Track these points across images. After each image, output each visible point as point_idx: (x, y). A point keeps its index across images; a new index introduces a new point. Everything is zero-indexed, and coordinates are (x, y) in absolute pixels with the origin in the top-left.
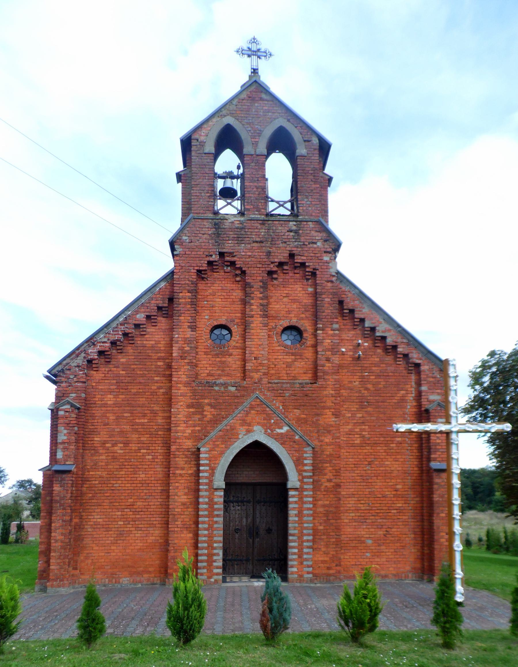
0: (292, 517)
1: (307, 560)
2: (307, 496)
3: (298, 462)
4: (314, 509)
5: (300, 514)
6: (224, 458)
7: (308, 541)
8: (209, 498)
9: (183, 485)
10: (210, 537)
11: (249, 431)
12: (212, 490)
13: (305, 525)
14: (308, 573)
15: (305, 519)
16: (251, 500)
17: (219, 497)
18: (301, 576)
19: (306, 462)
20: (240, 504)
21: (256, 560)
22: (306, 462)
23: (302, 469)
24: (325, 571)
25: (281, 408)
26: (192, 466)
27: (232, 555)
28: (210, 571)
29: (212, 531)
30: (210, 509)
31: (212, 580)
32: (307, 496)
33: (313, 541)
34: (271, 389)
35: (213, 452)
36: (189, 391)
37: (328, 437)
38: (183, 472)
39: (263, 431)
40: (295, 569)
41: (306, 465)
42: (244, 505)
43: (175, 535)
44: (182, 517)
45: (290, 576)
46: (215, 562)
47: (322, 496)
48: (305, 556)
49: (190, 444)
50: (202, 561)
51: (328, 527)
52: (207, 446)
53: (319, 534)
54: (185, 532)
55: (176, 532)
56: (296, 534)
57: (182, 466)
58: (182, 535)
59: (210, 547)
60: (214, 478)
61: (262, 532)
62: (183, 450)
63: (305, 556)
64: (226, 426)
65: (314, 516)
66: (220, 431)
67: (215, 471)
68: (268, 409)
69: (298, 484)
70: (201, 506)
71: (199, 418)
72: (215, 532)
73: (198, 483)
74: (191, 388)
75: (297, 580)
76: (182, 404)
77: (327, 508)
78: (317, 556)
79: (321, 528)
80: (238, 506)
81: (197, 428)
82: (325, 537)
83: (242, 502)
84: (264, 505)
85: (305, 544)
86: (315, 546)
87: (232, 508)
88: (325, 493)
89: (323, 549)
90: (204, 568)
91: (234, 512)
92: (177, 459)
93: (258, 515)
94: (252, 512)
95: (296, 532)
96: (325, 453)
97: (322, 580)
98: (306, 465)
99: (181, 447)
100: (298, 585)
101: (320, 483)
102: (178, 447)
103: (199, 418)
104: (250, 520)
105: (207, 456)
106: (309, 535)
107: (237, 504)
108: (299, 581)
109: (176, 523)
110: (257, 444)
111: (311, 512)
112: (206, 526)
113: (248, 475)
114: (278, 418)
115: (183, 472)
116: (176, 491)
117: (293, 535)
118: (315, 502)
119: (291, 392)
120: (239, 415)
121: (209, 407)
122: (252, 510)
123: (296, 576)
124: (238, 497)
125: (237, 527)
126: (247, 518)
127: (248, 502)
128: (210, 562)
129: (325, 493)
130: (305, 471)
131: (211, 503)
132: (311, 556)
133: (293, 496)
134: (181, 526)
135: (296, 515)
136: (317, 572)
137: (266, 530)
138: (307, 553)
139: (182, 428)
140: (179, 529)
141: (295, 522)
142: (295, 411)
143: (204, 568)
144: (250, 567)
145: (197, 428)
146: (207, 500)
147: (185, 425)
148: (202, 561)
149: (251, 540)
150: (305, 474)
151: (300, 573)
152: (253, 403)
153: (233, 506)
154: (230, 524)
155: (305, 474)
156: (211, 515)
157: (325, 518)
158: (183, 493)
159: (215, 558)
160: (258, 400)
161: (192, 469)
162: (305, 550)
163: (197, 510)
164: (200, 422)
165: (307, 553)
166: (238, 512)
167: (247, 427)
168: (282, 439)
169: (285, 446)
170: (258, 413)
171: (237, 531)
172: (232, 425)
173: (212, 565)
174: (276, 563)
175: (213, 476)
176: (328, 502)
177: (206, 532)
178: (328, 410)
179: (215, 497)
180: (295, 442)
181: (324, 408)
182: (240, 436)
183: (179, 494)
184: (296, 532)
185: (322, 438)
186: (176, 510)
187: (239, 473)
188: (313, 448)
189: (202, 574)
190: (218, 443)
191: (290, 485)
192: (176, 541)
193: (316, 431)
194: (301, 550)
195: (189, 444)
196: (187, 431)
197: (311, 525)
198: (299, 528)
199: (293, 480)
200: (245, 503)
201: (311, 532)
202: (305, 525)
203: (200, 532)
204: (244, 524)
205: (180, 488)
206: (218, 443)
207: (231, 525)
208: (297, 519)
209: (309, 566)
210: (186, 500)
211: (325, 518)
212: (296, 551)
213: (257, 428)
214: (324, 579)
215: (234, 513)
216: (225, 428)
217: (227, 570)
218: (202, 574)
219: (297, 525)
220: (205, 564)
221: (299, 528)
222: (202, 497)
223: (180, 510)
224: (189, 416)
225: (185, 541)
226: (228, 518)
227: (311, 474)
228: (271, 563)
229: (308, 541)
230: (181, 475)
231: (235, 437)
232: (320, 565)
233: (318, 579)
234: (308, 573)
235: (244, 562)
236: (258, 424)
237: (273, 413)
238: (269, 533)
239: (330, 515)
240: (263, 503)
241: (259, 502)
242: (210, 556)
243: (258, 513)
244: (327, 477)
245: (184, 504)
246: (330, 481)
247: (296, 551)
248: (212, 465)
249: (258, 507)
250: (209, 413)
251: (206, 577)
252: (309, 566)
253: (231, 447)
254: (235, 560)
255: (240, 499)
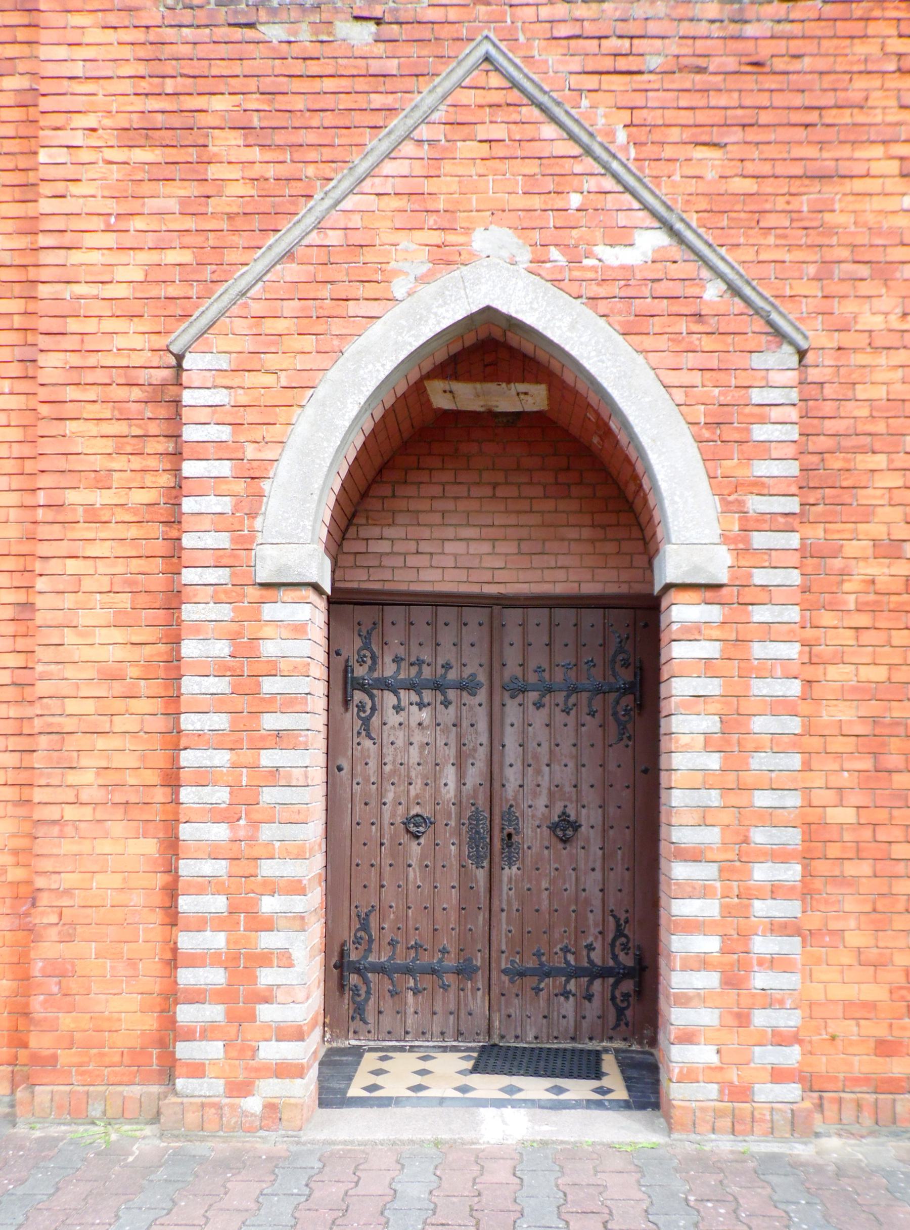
0: (687, 749)
1: (770, 1000)
2: (768, 632)
3: (721, 435)
4: (805, 708)
5: (731, 737)
6: (310, 410)
7: (775, 891)
8: (233, 638)
9: (102, 567)
10: (242, 856)
11: (445, 258)
12: (253, 593)
13: (762, 799)
14: (778, 1075)
15: (760, 762)
16: (482, 678)
17: (298, 635)
18: (740, 1093)
19: (760, 433)
20: (427, 696)
21: (505, 972)
22: (760, 433)
23: (740, 473)
24: (863, 1063)
25: (622, 136)
26: (152, 463)
27: (392, 943)
28: (241, 1050)
29: (255, 824)
30: (242, 703)
31: (253, 1104)
32: (768, 632)
33: (806, 892)
34: (563, 30)
35: (250, 379)
36: (126, 52)
37: (877, 304)
38: (100, 498)
39: (525, 256)
40: (703, 1054)
41: (763, 450)
42: (446, 703)
43: (67, 847)
44: (101, 743)
45: (676, 1092)
46: (267, 1000)
47: (848, 637)
48: (761, 980)
49: (138, 342)
50: (197, 996)
51: (881, 815)
52: (221, 343)
53: (833, 850)
54: (117, 829)
55: (69, 830)
56: (709, 847)
57: (99, 463)
58: (104, 846)
59: (244, 916)
60: (258, 523)
61: (532, 835)
62: (100, 376)
63: (761, 980)
64: (318, 227)
65: (812, 743)
66: (289, 255)
67: (266, 485)
68: (549, 131)
69: (718, 565)
70: (190, 685)
71: (184, 201)
72: (267, 832)
73: (175, 557)
74: (139, 35)
75: (718, 1114)
76: (90, 121)
77: (872, 708)
78: (823, 973)
79: (845, 815)
80: (421, 705)
81: (172, 257)
82: (865, 868)
83: (437, 686)
84: (538, 705)
85: (760, 907)
86: (814, 921)
87: (393, 718)
88: (863, 620)
89: (854, 939)
90: (207, 1032)
91: (400, 738)
92: (71, 427)
93: (512, 752)
94: (484, 739)
95: (711, 836)
96: (861, 392)
97: (848, 1114)
98: (763, 450)
99: (92, 360)
100: (723, 1145)
101: (837, 563)
102: (75, 360)
103: (184, 201)
104: (475, 774)
105: (220, 397)
106: (779, 856)
107: (415, 698)
108: (727, 1122)
109: (73, 778)
110: (490, 347)
111: (794, 725)
112: (220, 795)
113: (461, 550)
114: (608, 184)
115: (100, 498)
116: (69, 601)
117: (695, 856)
118: (811, 672)
119: (673, 47)
120: (389, 168)
121: (235, 138)
122: (482, 726)
123: (712, 1090)
124: (419, 663)
125: (416, 810)
126: (460, 765)
127: (467, 686)
128: (242, 999)
129: (863, 620)
130: (760, 487)
131: (246, 667)
132: (791, 981)
133: (694, 633)
134: (97, 795)
135: (709, 743)
136: (821, 1064)
137: (553, 828)
138: (773, 963)
139: (95, 257)
140: (87, 813)
141: (706, 780)
142: (701, 153)
143: (207, 1032)
144: (478, 1003)
145: (172, 257)
146: (222, 649)
147: (110, 240)
148: (197, 996)
149: (481, 875)
150: (757, 504)
151: (733, 1075)
152: (468, 97)
153: (398, 709)
154: (381, 793)
155: (757, 504)
156: (244, 737)
157: (867, 764)
158: (107, 616)
159: (267, 977)
160: (495, 80)
161: (149, 479)
162: (762, 945)
163: (173, 704)
164: (190, 223)
165: (773, 963)
166: (418, 737)
167: (436, 237)
168: (631, 305)
169: (648, 342)
170: (495, 152)
171: (415, 826)
172: (356, 221)
173: (253, 1018)
174: (597, 984)
175: (252, 515)
176: (879, 674)
177: (220, 832)
178: (878, 151)
179: (268, 631)
180: (698, 316)
181: (856, 136)
182: (399, 288)
183: (84, 618)
184: (711, 836)
185: (850, 307)
186: (72, 706)
187: (424, 547)
188: (802, 354)
189: (197, 1070)
190: (280, 326)
191: (673, 565)
192: (69, 880)
193: (812, 270)
194: (736, 942)
195: (132, 341)
196: (122, 274)
197: (793, 800)
198: (727, 817)
199: (691, 535)
200: (452, 694)
201: (793, 837)
202: (762, 799)
203: (186, 831)
204: (449, 792)
205: (88, 584)
206: (280, 326)
207: (389, 797)
208: (714, 761)
209: (780, 1039)
210: (119, 653)
211: (867, 764)
212: (710, 944)
213: (491, 240)
214: (859, 1106)
215: (400, 743)
216: (314, 238)
217: (371, 1017)
218: (197, 1070)
219: (714, 798)
220: (214, 1012)
221: (727, 817)
222: (197, 628)
223: (89, 707)
224: (131, 190)
225: (116, 881)
226: (373, 764)
227: (792, 505)
228: (572, 986)
229: (775, 891)
230: (93, 516)
231: (370, 290)
232: (834, 1027)
233: (830, 1110)
234: (778, 1075)
235: (449, 979)
236: (497, 213)
237: (576, 150)
238: (565, 841)
239: (895, 744)
240: (533, 696)
241: (518, 689)
242: (243, 963)
243: (511, 738)
244: (877, 530)
245: (110, 676)
246: (889, 549)
247: (710, 944)
248: (250, 452)
249: (512, 712)
250: (235, 165)
251: (219, 1086)
252: (780, 1039)
253: (351, 350)
254: (408, 971)
255: (427, 672)
